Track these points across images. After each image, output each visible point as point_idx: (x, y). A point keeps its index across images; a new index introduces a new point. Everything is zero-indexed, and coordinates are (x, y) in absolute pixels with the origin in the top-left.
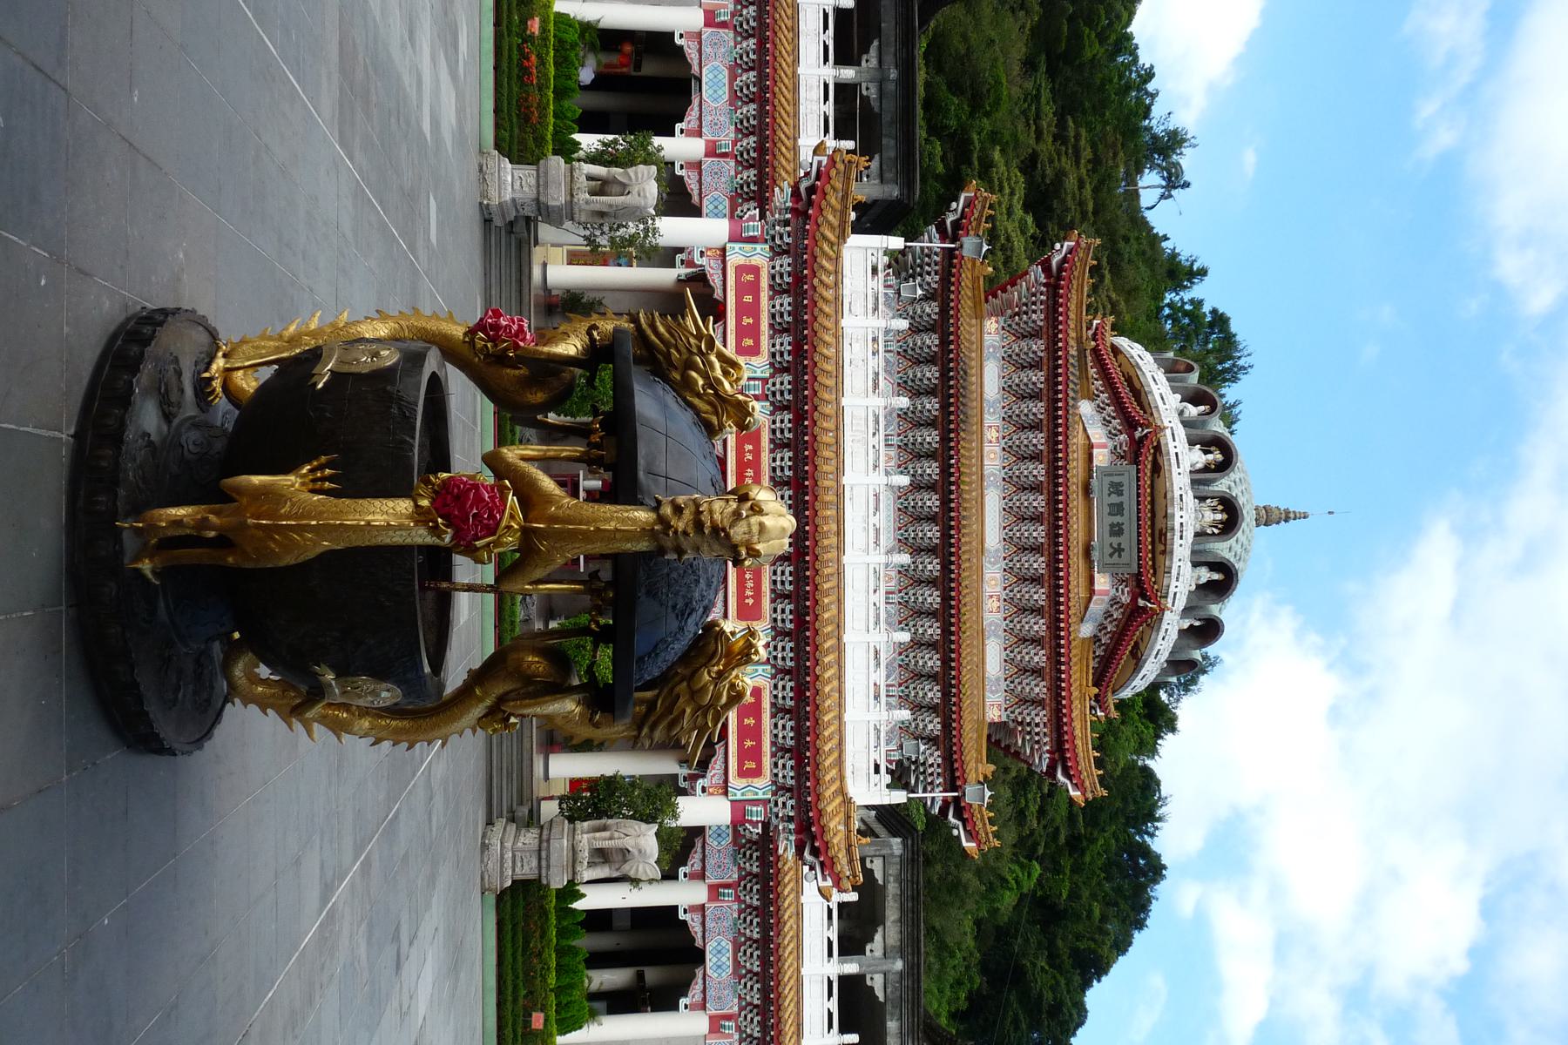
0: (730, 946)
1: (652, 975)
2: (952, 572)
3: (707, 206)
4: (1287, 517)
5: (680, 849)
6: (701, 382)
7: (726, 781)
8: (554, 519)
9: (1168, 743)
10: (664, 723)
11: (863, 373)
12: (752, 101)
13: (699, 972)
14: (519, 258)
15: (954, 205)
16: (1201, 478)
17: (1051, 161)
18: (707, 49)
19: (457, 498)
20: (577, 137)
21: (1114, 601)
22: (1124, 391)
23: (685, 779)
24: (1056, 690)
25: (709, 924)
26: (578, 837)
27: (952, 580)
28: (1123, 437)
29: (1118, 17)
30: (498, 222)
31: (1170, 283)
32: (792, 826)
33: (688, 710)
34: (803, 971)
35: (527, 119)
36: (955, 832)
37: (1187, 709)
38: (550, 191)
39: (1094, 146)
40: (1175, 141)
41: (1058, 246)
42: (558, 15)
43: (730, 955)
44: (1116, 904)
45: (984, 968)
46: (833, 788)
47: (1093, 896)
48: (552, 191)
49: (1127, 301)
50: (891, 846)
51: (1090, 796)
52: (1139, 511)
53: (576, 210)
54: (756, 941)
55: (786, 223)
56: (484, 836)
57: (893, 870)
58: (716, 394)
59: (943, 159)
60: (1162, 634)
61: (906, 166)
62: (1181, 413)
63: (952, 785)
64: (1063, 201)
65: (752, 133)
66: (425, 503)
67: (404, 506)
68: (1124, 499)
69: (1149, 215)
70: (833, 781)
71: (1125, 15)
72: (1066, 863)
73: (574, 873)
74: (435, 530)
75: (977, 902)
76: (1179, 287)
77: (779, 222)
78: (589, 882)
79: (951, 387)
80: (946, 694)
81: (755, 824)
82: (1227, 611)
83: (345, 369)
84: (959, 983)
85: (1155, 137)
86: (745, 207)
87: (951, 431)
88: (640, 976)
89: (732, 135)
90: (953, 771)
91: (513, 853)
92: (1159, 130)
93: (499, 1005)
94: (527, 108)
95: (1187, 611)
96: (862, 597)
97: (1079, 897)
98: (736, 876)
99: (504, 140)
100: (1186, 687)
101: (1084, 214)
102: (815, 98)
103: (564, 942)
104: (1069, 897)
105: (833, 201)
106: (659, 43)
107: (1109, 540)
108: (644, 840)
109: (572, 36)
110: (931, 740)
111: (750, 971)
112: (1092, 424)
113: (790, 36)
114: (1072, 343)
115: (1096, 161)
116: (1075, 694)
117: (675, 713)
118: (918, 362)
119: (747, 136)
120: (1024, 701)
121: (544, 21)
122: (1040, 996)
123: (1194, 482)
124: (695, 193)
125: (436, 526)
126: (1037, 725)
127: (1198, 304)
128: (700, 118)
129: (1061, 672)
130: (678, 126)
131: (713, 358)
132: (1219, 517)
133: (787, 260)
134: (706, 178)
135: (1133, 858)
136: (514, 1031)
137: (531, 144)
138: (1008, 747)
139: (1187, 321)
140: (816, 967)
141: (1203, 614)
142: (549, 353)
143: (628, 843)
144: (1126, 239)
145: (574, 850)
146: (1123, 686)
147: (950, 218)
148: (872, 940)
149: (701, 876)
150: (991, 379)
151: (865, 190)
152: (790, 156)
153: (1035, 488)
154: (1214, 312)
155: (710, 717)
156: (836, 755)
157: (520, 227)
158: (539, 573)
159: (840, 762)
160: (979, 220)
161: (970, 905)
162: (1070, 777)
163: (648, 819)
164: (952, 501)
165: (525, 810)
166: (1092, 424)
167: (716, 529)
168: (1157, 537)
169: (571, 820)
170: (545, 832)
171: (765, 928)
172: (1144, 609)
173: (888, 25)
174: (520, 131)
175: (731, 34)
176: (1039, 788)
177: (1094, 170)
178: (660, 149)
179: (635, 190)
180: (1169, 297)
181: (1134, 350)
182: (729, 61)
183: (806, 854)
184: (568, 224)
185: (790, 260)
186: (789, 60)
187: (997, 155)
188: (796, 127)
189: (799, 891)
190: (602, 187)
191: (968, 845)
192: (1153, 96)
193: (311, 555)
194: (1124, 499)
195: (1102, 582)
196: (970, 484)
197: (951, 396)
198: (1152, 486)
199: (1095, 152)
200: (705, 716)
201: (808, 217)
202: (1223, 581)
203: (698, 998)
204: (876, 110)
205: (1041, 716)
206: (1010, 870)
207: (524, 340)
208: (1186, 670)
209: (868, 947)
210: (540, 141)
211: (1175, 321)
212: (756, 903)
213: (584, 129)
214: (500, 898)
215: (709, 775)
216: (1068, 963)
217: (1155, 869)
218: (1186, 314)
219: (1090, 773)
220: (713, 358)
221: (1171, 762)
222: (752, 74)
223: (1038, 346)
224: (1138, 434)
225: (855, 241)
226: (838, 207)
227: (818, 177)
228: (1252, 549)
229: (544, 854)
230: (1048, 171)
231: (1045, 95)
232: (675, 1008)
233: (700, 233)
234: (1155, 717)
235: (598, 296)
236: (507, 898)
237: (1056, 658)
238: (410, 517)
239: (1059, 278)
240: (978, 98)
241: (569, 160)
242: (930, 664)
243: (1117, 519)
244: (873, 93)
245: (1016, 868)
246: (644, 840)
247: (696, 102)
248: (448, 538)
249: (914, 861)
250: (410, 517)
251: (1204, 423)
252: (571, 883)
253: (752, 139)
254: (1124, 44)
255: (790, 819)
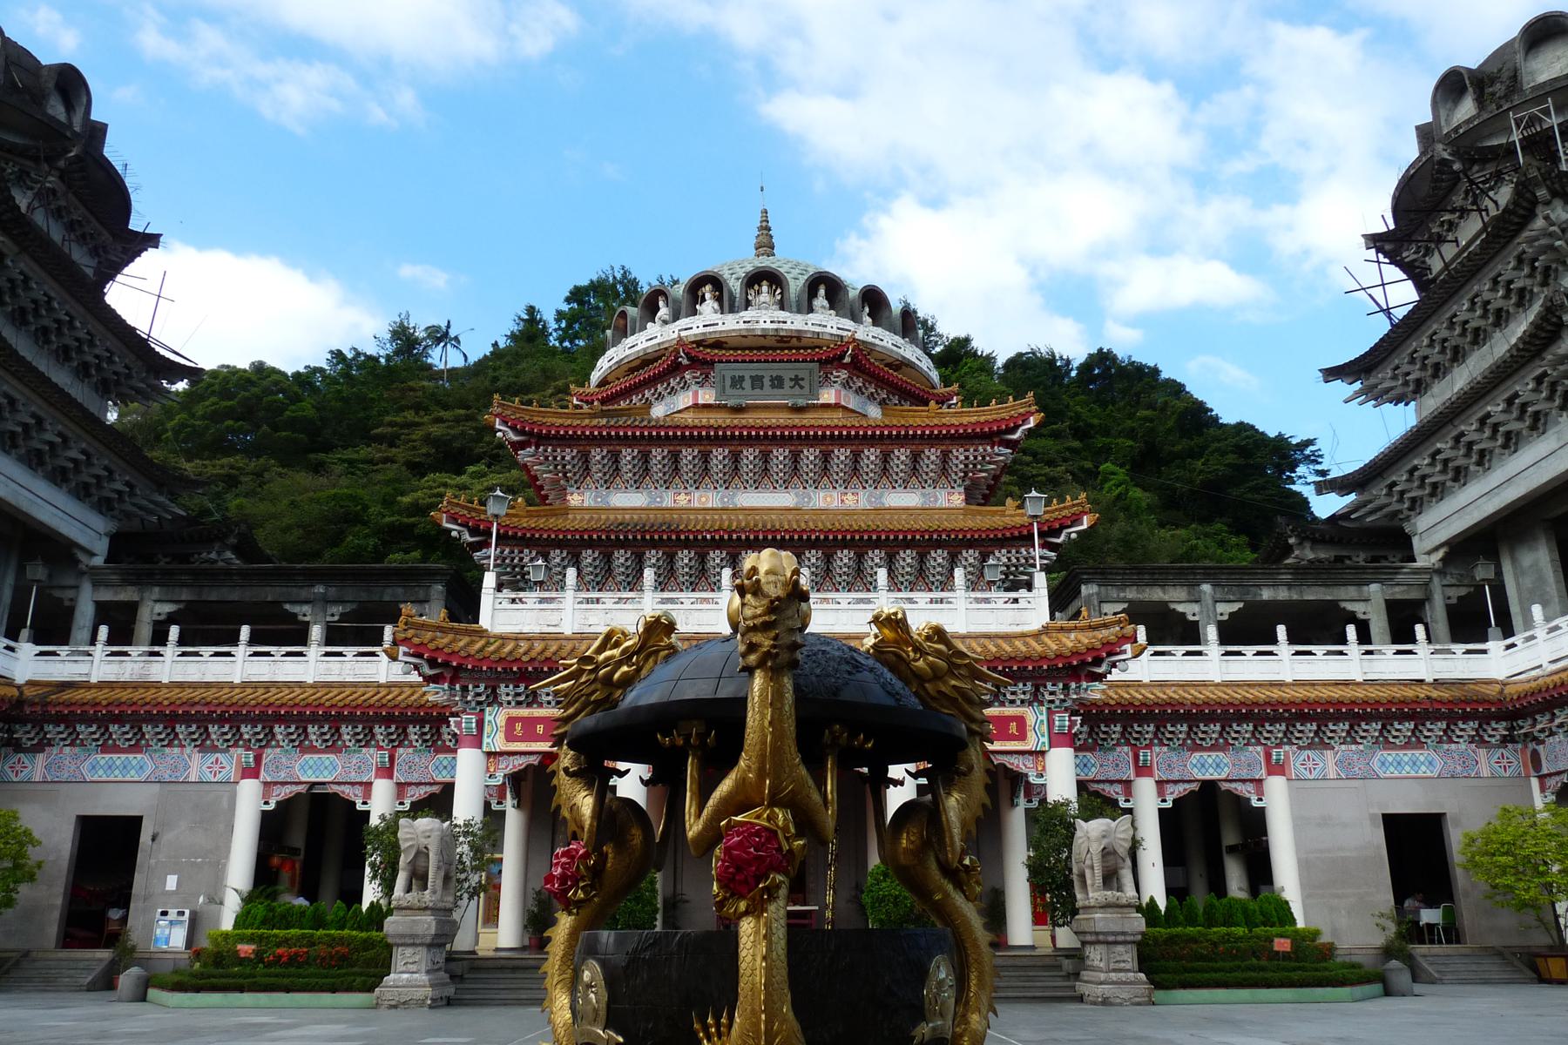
0: (1197, 755)
1: (1230, 838)
2: (818, 538)
3: (443, 777)
4: (765, 228)
5: (1095, 800)
6: (625, 668)
7: (1030, 753)
8: (761, 774)
9: (981, 345)
10: (966, 706)
11: (619, 614)
12: (338, 730)
13: (1225, 786)
14: (488, 969)
15: (454, 534)
16: (727, 304)
17: (414, 448)
18: (282, 776)
19: (739, 869)
20: (365, 906)
21: (846, 385)
22: (643, 374)
23: (1030, 801)
24: (932, 440)
25: (1176, 776)
26: (1092, 902)
27: (826, 538)
28: (688, 376)
29: (276, 383)
30: (450, 991)
31: (540, 340)
32: (1073, 685)
33: (953, 682)
34: (1218, 680)
35: (344, 958)
36: (1074, 536)
37: (949, 328)
38: (420, 932)
39: (402, 409)
40: (403, 337)
41: (499, 434)
42: (236, 925)
43: (1205, 754)
44: (1138, 395)
45: (1206, 520)
46: (1034, 644)
47: (1131, 416)
48: (420, 930)
49: (556, 379)
50: (1090, 596)
51: (1034, 408)
52: (759, 361)
53: (440, 905)
54: (1190, 728)
55: (465, 689)
56: (1095, 1003)
57: (1113, 593)
58: (637, 653)
59: (407, 552)
60: (877, 342)
61: (412, 578)
62: (665, 322)
63: (1028, 539)
64: (455, 437)
65: (371, 730)
66: (742, 906)
67: (747, 927)
68: (747, 375)
69: (473, 359)
70: (1026, 644)
71: (274, 377)
72: (1100, 441)
73: (1129, 906)
74: (771, 892)
75: (1141, 523)
76: (544, 333)
77: (464, 697)
78: (1138, 891)
79: (635, 538)
80: (939, 544)
81: (1072, 724)
82: (855, 278)
83: (603, 1013)
84: (1222, 544)
85: (397, 352)
86: (446, 737)
87: (678, 538)
88: (1232, 850)
89: (372, 750)
90: (1013, 538)
91: (1110, 972)
92: (390, 349)
93: (1269, 986)
94: (332, 957)
95: (856, 318)
96: (844, 616)
97: (1133, 429)
98: (1126, 749)
99: (364, 983)
100: (929, 329)
101: (468, 418)
102: (338, 665)
103: (1201, 919)
104: (1133, 438)
105: (445, 641)
106: (272, 827)
107: (787, 390)
108: (1092, 833)
109: (260, 910)
110: (984, 558)
111: (1221, 734)
112: (675, 404)
113: (274, 691)
114: (595, 422)
115: (417, 407)
116: (936, 421)
117: (956, 695)
118: (609, 571)
119: (373, 736)
120: (944, 470)
121: (242, 939)
122: (1228, 465)
123: (732, 310)
124: (429, 789)
125: (766, 889)
126: (967, 458)
127: (560, 315)
128: (353, 784)
129: (915, 435)
130: (360, 807)
131: (601, 657)
132: (765, 288)
133: (502, 689)
134: (415, 778)
135: (1093, 379)
136: (1294, 970)
137: (370, 954)
138: (989, 487)
139: (577, 326)
140: (1212, 667)
141: (858, 304)
142: (592, 817)
143: (1096, 849)
144: (495, 379)
145: (1106, 906)
146: (928, 379)
147: (467, 537)
148: (1183, 614)
149: (1127, 784)
150: (628, 500)
151: (436, 613)
152: (396, 691)
153: (736, 458)
154: (568, 300)
155: (959, 661)
156: (1000, 641)
157: (457, 968)
158: (816, 797)
159: (1007, 637)
160: (470, 510)
161: (1144, 529)
162: (1017, 427)
163: (1071, 829)
164: (747, 538)
165: (1067, 964)
166: (675, 404)
167: (771, 609)
168: (783, 345)
169: (1075, 912)
170: (1089, 938)
171: (1176, 718)
172: (853, 357)
173: (270, 594)
174: (355, 965)
175: (269, 751)
176: (1028, 464)
177: (426, 409)
178: (383, 817)
179: (424, 841)
180: (553, 342)
181: (604, 365)
182: (295, 753)
183: (1100, 670)
184: (456, 916)
185: (503, 686)
186: (298, 691)
187: (406, 500)
188: (367, 685)
189: (1138, 684)
190: (418, 878)
191: (1085, 524)
192: (358, 354)
193: (796, 1026)
194: (747, 375)
195: (828, 396)
196: (730, 520)
197: (643, 538)
198: (735, 349)
199: (409, 408)
200: (959, 666)
201: (460, 666)
202: (826, 286)
203: (1250, 787)
204: (354, 606)
205: (959, 454)
206: (1110, 492)
207: (577, 851)
208: (909, 323)
209: (1191, 618)
210: (368, 944)
211: (576, 336)
212: (1152, 728)
213: (358, 896)
214: (1159, 986)
215: (1024, 770)
216: (1198, 440)
217: (1103, 359)
218: (569, 326)
219: (1010, 408)
220: (601, 657)
221: (1000, 342)
222: (310, 729)
223: (597, 454)
224: (685, 362)
225: (485, 621)
226: (451, 636)
227: (420, 656)
228: (796, 258)
229: (1111, 938)
230: (424, 451)
231: (349, 454)
232: (1263, 809)
233: (470, 778)
234: (957, 357)
235: (531, 895)
236: (1157, 978)
237: (902, 440)
238: (758, 917)
239: (531, 434)
240: (348, 517)
241: (390, 912)
242: (909, 560)
243: (767, 382)
244: (337, 610)
245: (1107, 486)
246: (1092, 833)
247: (336, 788)
248: (779, 878)
249: (1103, 575)
250: (758, 917)
251: (676, 301)
252: (1139, 909)
253: (377, 730)
254: (304, 380)
255: (1066, 687)
